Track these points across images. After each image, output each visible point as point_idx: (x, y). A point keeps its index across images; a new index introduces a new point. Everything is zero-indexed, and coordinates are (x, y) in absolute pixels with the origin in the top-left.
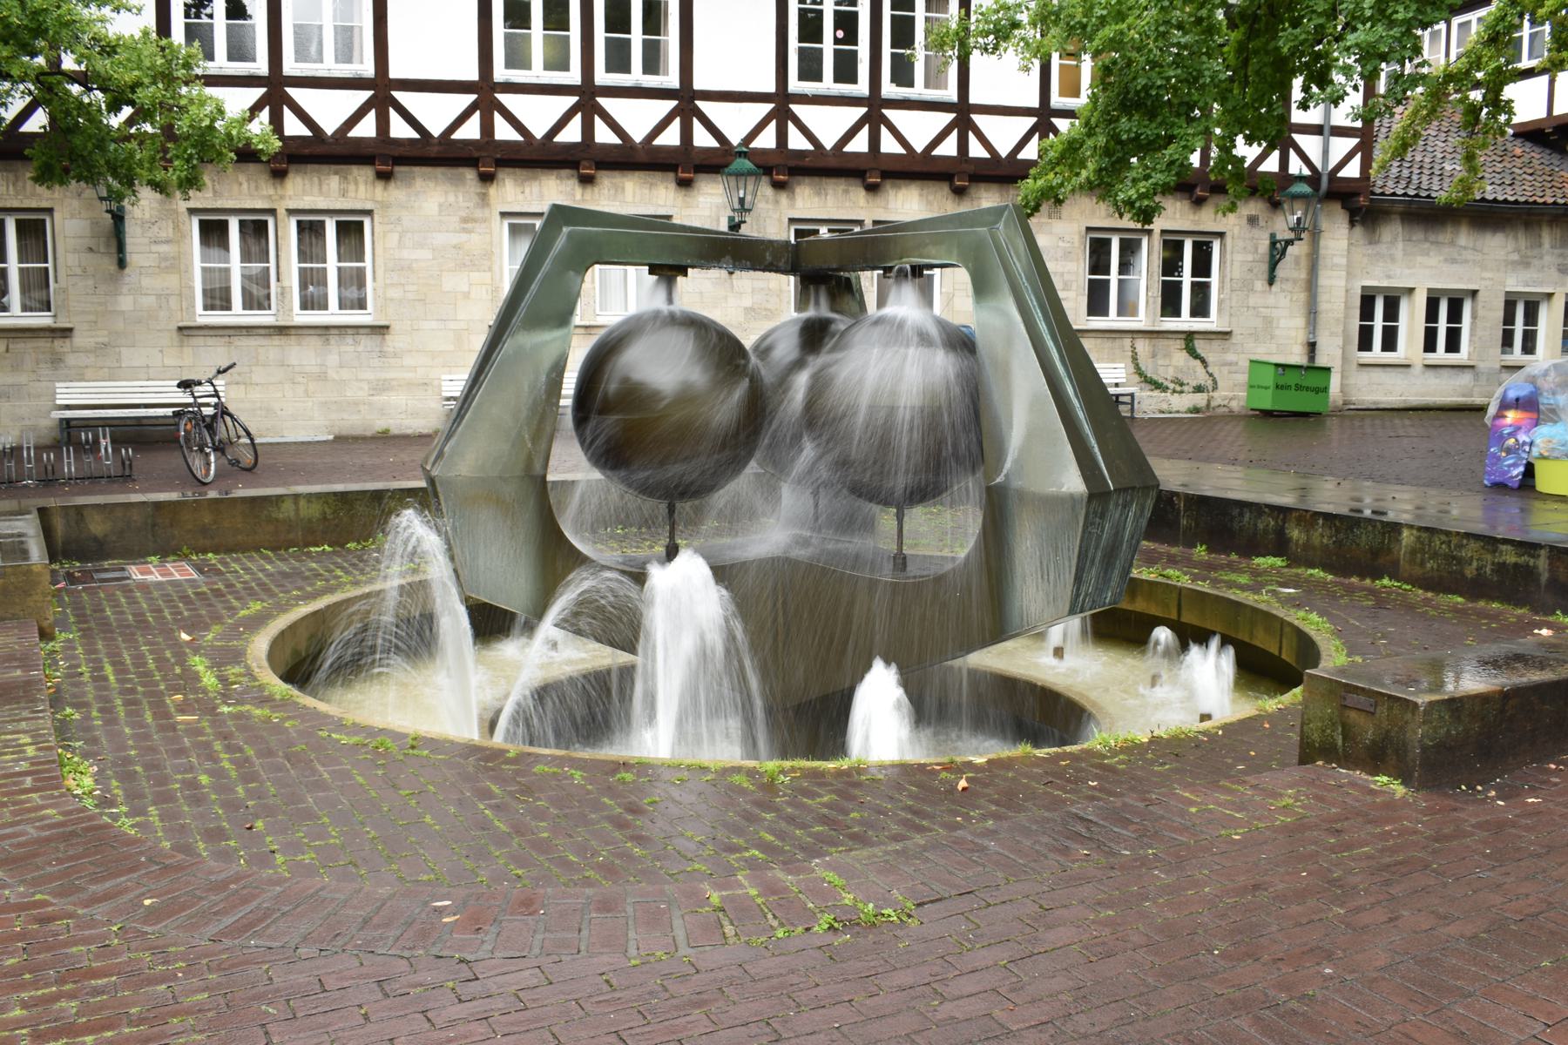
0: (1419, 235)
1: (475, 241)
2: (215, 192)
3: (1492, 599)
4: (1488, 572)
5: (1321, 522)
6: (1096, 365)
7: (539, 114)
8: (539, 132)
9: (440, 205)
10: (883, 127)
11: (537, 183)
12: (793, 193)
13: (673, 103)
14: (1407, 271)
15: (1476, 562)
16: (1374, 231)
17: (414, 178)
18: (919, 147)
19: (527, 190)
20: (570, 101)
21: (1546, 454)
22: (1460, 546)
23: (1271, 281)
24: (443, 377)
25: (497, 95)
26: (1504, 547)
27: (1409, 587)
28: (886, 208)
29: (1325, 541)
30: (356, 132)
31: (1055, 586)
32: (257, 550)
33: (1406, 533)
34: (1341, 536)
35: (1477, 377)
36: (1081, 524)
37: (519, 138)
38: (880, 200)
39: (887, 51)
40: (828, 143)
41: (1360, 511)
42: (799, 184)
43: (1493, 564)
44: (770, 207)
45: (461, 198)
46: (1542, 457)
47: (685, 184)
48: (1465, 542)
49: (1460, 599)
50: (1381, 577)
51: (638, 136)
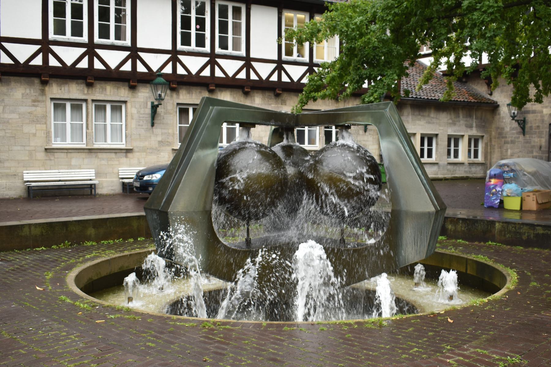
0: (417, 113)
1: (39, 110)
3: (534, 247)
4: (532, 237)
5: (461, 222)
9: (23, 94)
10: (95, 58)
11: (67, 85)
13: (128, 53)
14: (413, 127)
15: (526, 233)
16: (401, 111)
17: (10, 82)
18: (231, 74)
19: (63, 89)
20: (83, 50)
21: (509, 195)
22: (520, 228)
23: (153, 125)
24: (24, 172)
25: (50, 46)
26: (538, 228)
27: (500, 244)
29: (463, 229)
31: (420, 247)
32: (13, 250)
33: (497, 224)
34: (470, 227)
35: (439, 167)
36: (432, 223)
37: (60, 65)
39: (179, 30)
40: (194, 72)
41: (476, 217)
42: (181, 89)
43: (534, 234)
44: (169, 98)
45: (32, 91)
46: (508, 196)
47: (133, 88)
48: (522, 226)
49: (521, 248)
50: (488, 241)
51: (113, 66)
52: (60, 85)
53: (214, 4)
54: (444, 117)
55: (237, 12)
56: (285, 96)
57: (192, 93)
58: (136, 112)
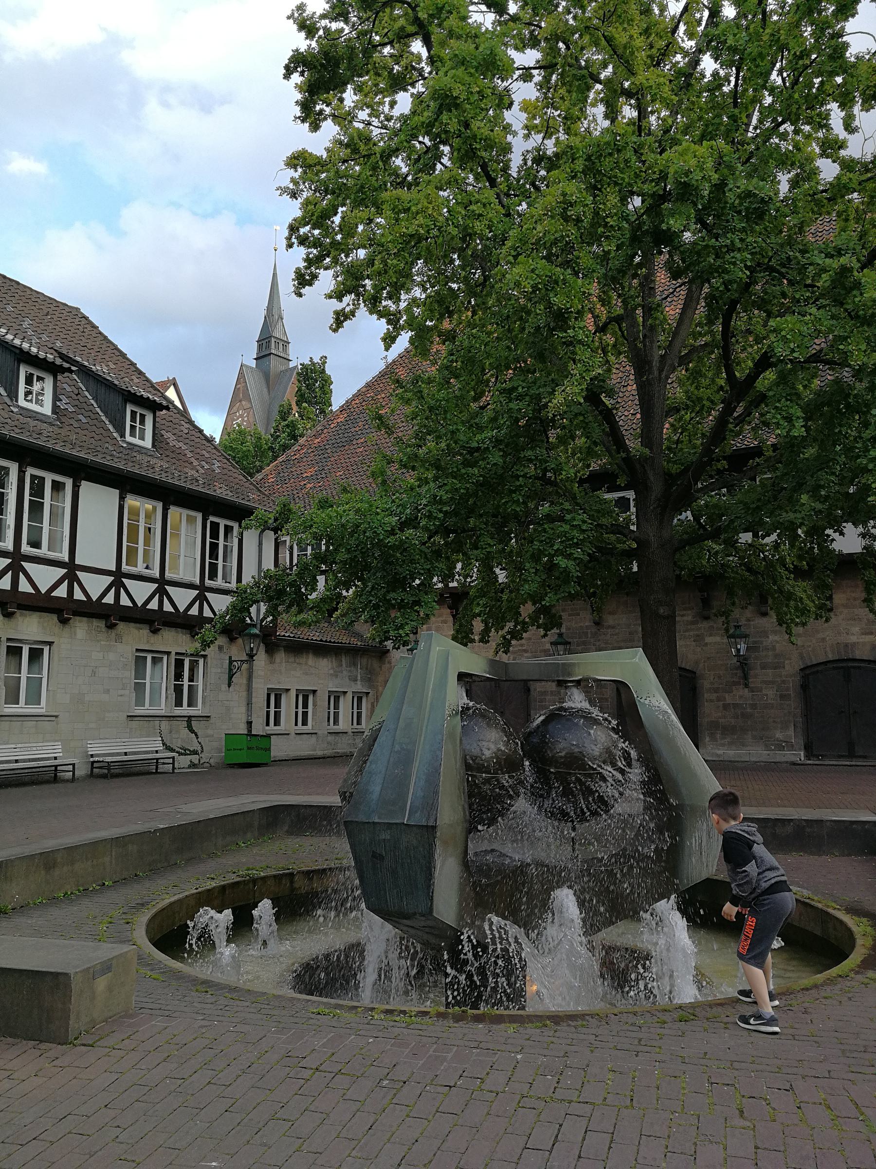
0: (292, 659)
23: (229, 686)
47: (64, 621)
53: (24, 472)
54: (325, 665)
55: (57, 487)
56: (122, 626)
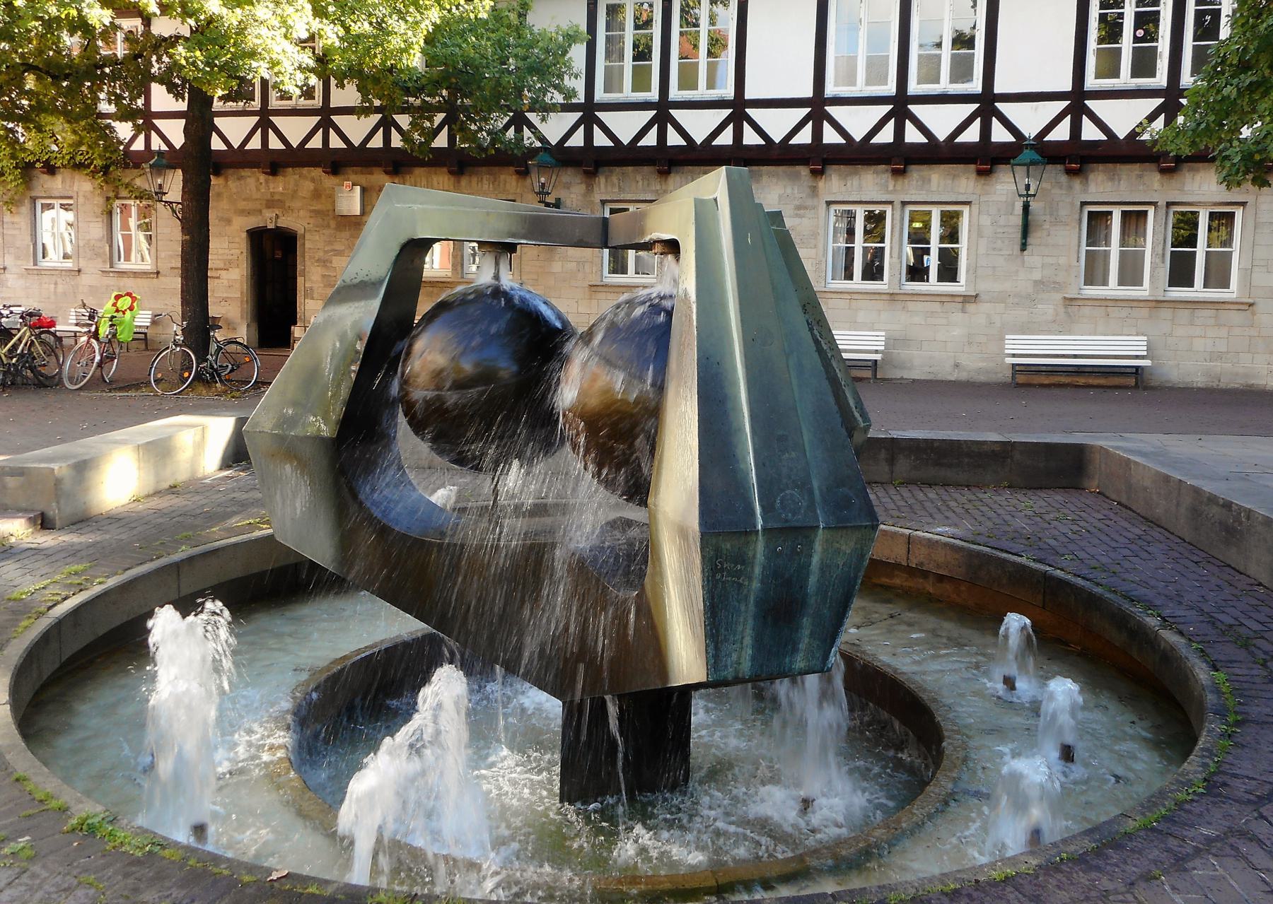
2: (620, 187)
6: (834, 332)
7: (626, 126)
8: (858, 136)
9: (780, 196)
12: (1087, 179)
18: (626, 140)
19: (849, 184)
23: (1024, 247)
24: (1007, 337)
28: (1181, 190)
30: (718, 141)
38: (1175, 181)
52: (844, 177)
57: (1120, 180)
58: (988, 223)
